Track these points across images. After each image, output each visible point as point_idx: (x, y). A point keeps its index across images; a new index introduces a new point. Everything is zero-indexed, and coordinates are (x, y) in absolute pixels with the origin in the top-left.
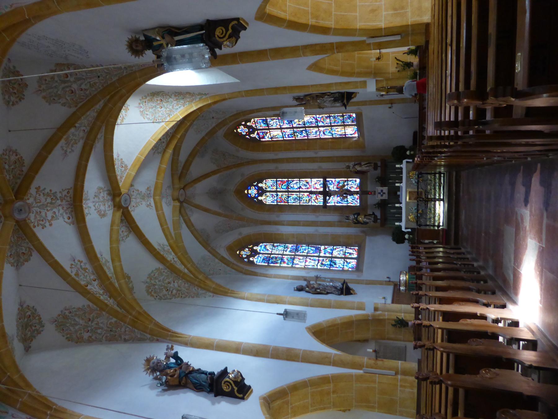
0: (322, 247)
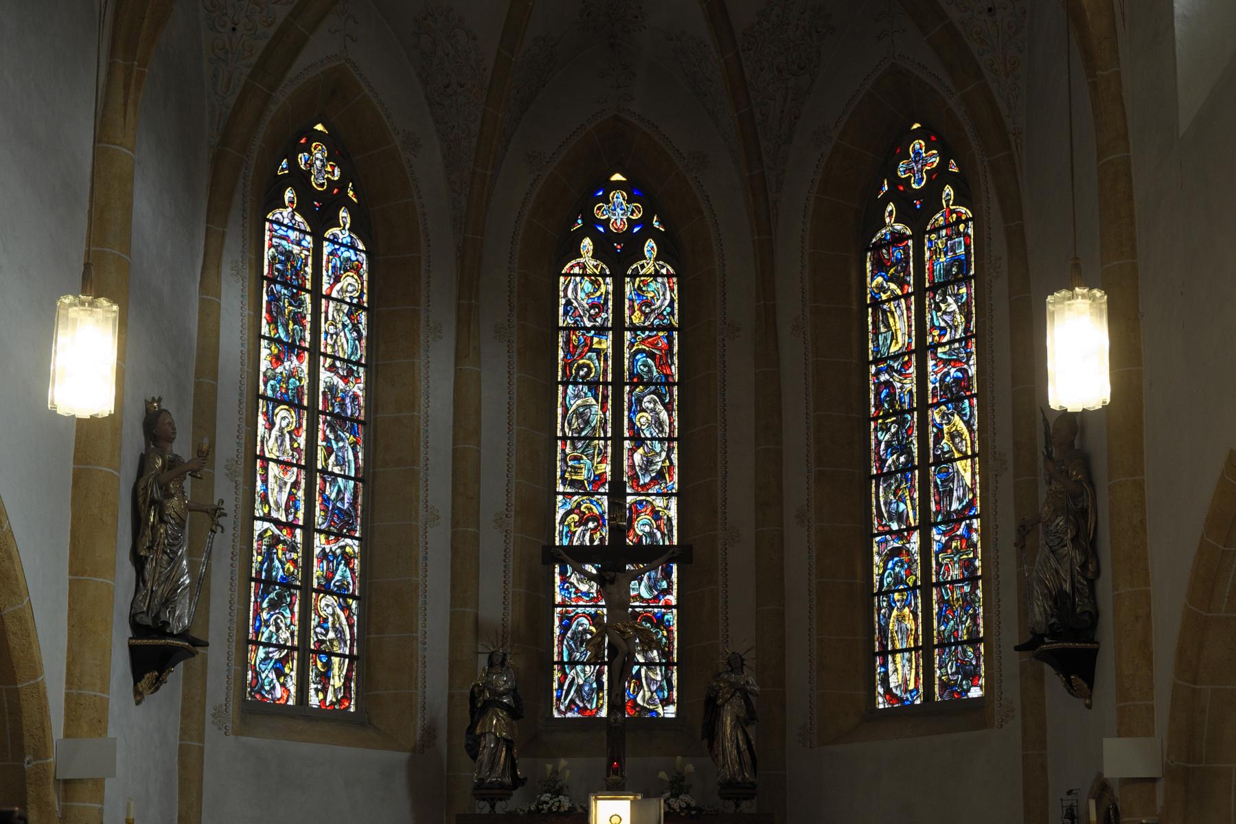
0: (352, 546)
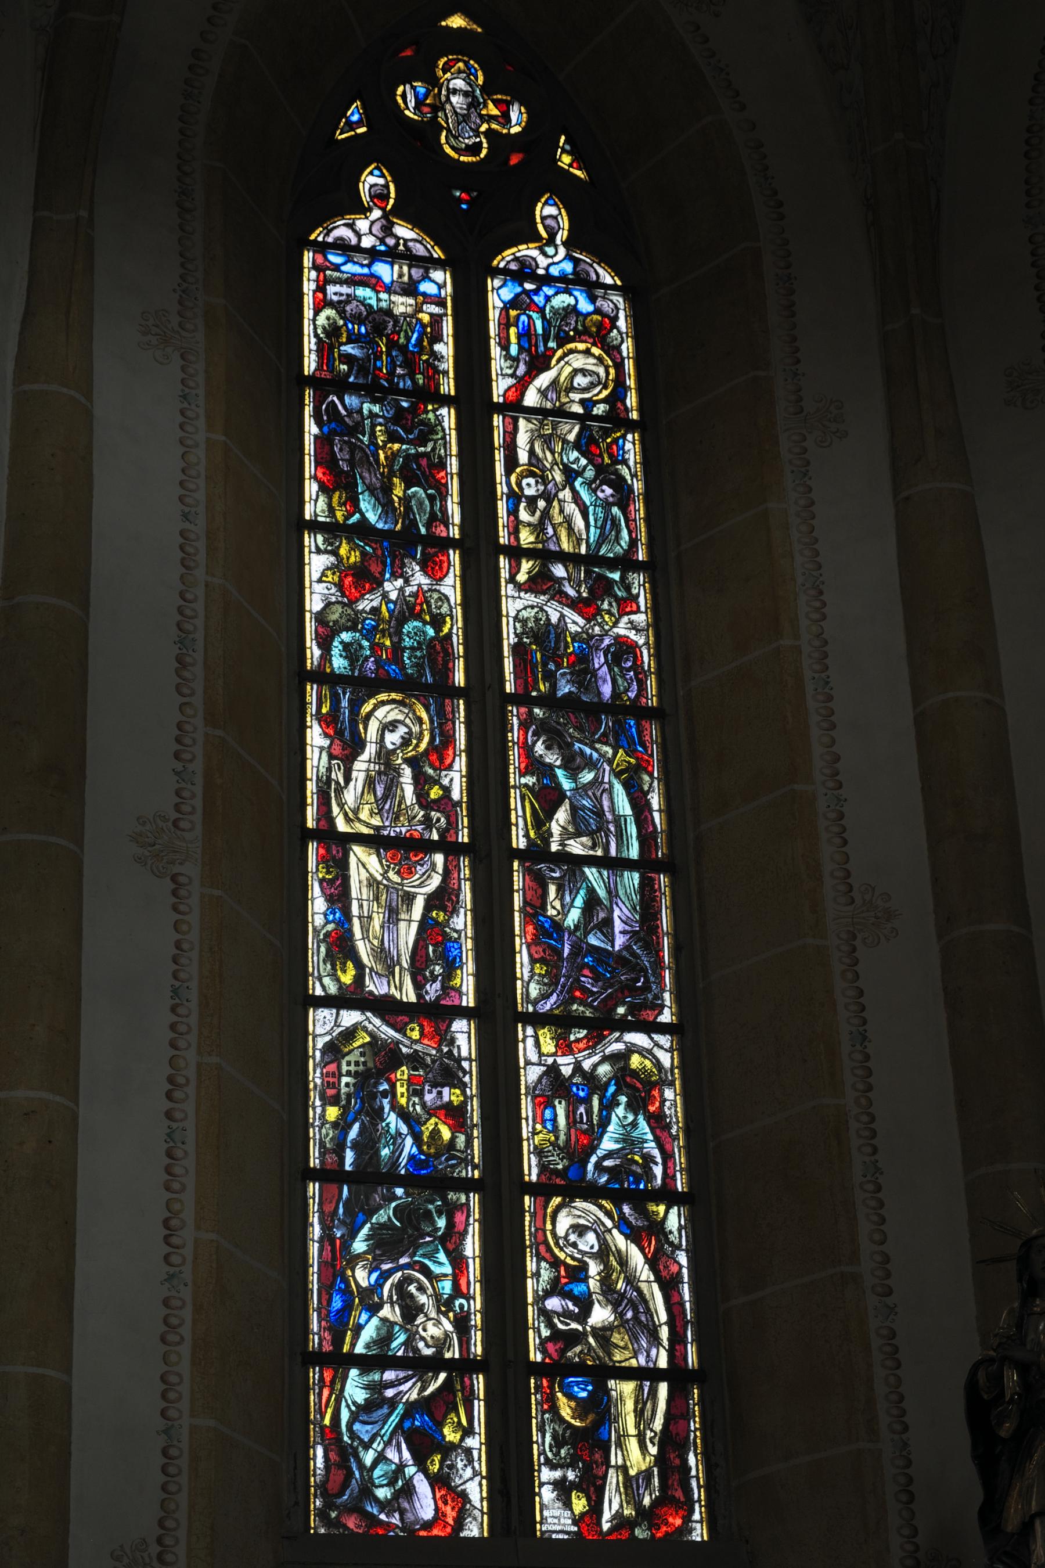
0: (655, 1051)
